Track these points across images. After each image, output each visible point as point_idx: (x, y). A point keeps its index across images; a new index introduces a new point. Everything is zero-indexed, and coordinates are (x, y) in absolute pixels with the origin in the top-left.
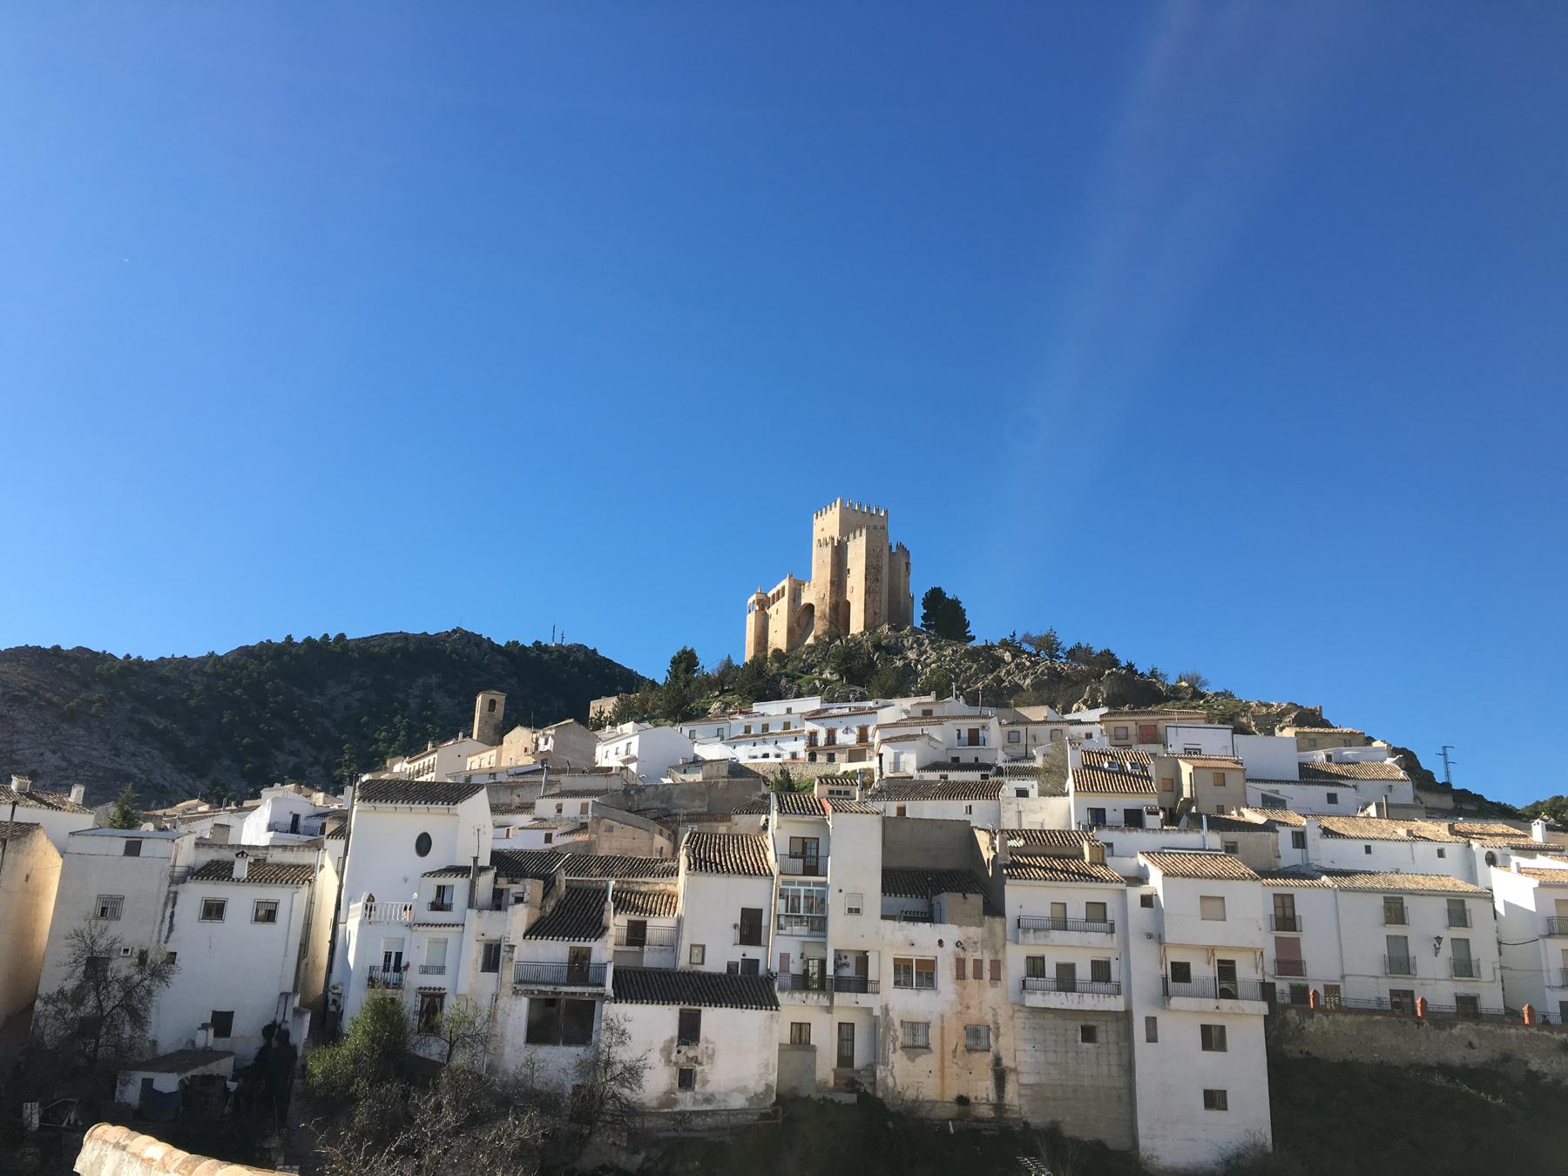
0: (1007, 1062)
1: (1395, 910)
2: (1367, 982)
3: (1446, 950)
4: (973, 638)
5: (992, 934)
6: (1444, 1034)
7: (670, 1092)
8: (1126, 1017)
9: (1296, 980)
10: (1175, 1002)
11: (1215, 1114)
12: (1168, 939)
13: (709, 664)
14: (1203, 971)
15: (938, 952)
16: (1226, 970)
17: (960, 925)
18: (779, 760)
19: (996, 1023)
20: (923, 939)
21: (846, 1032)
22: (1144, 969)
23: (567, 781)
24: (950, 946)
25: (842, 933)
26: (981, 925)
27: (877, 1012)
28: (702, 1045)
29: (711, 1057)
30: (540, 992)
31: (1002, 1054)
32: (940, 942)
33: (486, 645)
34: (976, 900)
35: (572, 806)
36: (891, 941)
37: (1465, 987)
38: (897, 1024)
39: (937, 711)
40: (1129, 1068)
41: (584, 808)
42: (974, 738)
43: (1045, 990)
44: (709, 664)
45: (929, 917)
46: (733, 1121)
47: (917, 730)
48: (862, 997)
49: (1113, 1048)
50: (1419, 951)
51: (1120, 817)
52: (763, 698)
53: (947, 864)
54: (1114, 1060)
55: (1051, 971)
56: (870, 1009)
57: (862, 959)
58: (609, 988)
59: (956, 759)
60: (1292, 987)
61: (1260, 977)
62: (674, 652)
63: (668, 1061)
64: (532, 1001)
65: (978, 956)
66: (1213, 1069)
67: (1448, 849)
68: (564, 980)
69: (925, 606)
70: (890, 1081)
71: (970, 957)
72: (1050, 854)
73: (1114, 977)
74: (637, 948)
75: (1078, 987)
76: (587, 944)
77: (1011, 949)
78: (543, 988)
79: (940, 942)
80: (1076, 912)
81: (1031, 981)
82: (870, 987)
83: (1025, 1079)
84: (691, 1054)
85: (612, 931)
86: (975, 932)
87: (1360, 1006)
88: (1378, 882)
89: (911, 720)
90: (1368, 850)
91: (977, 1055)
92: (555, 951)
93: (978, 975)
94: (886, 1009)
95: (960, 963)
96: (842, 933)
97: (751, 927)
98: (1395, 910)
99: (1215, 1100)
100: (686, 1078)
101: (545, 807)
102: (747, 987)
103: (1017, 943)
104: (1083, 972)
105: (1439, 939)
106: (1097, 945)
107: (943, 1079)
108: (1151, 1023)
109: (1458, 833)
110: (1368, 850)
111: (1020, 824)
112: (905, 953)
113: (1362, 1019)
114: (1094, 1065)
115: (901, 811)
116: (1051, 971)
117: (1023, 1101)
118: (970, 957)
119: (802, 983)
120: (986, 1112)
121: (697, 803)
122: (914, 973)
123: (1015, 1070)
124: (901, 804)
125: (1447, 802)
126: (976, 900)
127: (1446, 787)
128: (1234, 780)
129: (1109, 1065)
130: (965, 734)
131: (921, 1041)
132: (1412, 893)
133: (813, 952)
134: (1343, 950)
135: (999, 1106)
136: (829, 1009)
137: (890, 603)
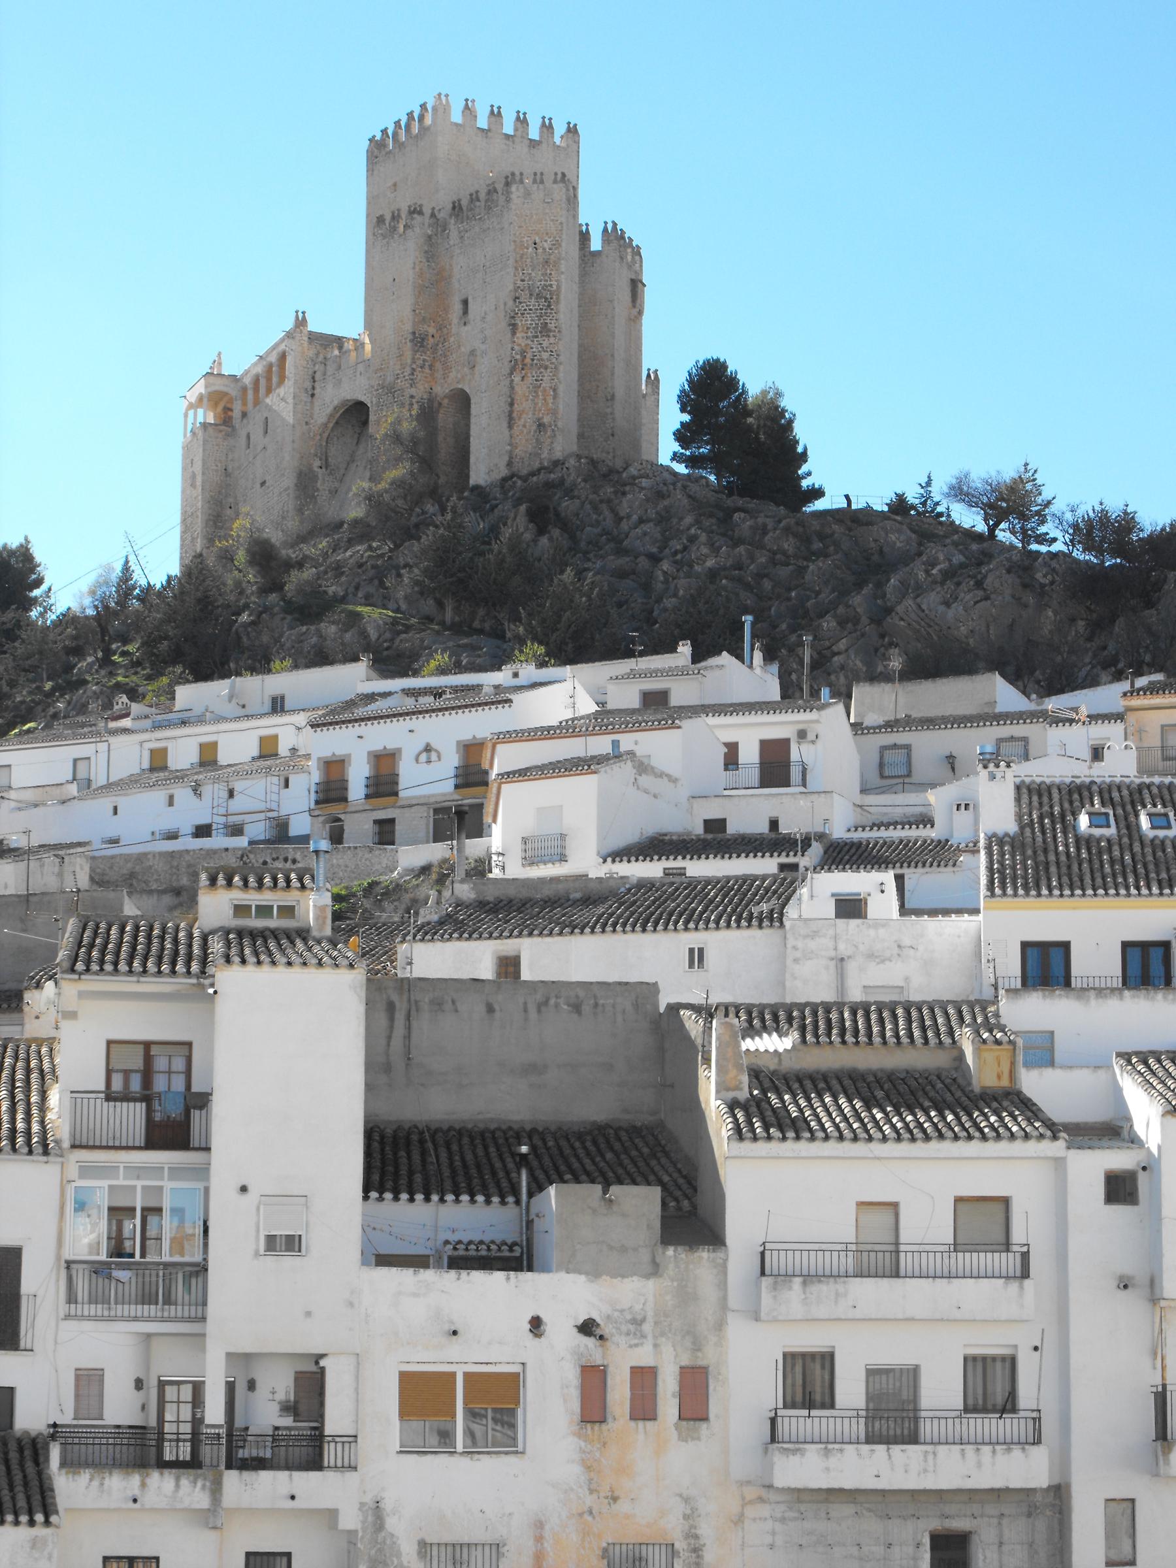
4: (817, 493)
5: (686, 1295)
8: (1056, 1500)
17: (595, 1274)
20: (487, 1318)
25: (253, 1310)
26: (655, 1270)
27: (350, 1520)
32: (536, 1324)
34: (641, 1203)
39: (682, 693)
42: (776, 767)
43: (827, 1443)
45: (516, 1257)
47: (600, 745)
48: (305, 1483)
53: (594, 1107)
55: (851, 1390)
56: (332, 1515)
57: (311, 1385)
59: (715, 826)
65: (644, 1356)
69: (685, 403)
71: (622, 1360)
73: (1026, 1397)
75: (927, 1429)
77: (738, 1331)
79: (536, 1324)
80: (928, 1223)
81: (795, 1422)
82: (330, 1453)
86: (632, 1293)
89: (604, 719)
93: (644, 1409)
94: (376, 1513)
95: (593, 1379)
96: (253, 1310)
104: (942, 1389)
108: (1123, 1515)
111: (841, 986)
112: (431, 1358)
115: (509, 966)
118: (622, 1360)
119: (141, 1449)
122: (468, 1409)
124: (508, 946)
126: (641, 1203)
130: (749, 754)
136: (211, 1517)
137: (585, 395)
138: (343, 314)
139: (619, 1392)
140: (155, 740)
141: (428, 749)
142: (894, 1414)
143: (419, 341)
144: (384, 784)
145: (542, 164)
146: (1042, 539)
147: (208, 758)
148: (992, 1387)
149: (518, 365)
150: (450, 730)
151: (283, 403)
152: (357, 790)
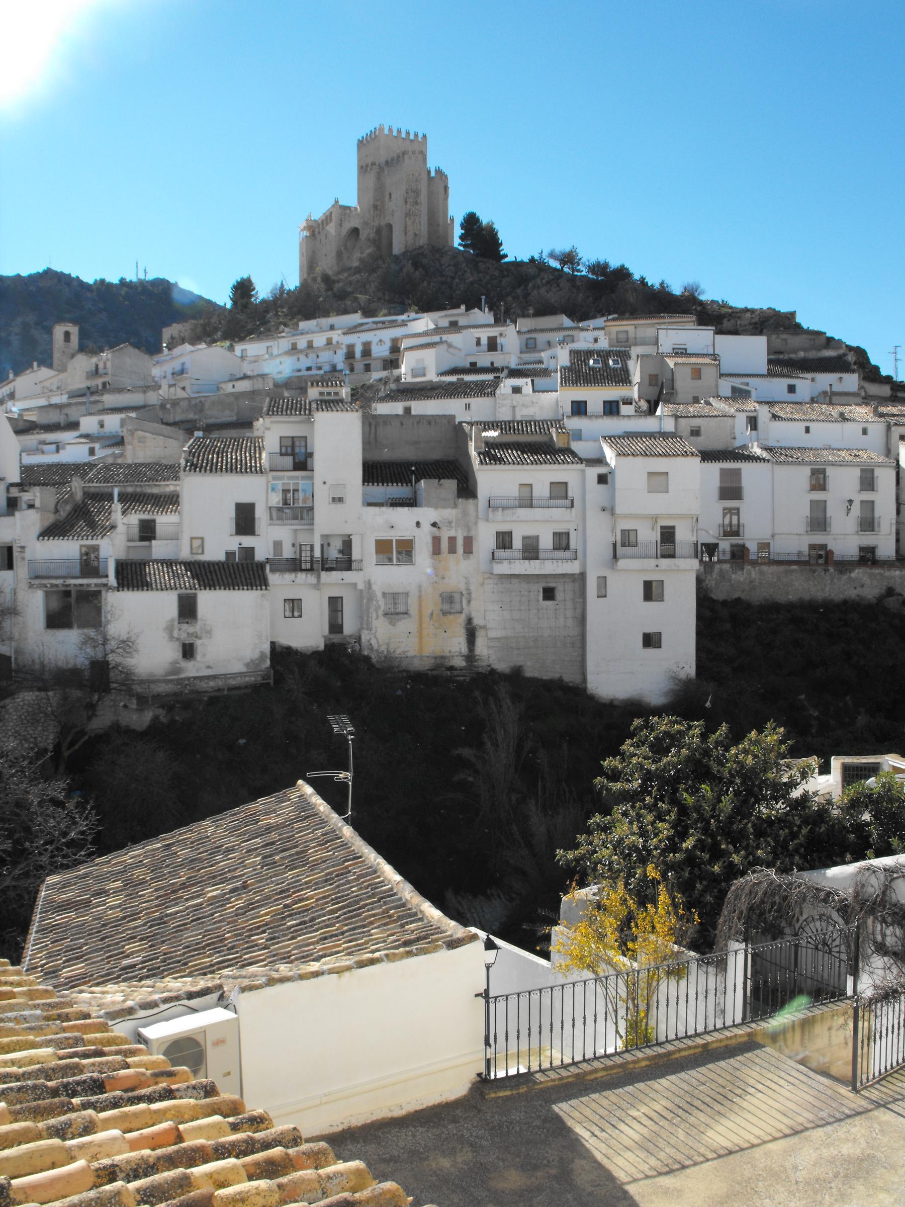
0: (477, 621)
1: (819, 481)
2: (793, 540)
3: (856, 510)
5: (465, 514)
6: (845, 577)
7: (175, 662)
8: (581, 578)
9: (735, 540)
10: (622, 563)
11: (651, 651)
12: (618, 510)
13: (263, 291)
14: (649, 536)
15: (416, 532)
16: (668, 535)
17: (436, 507)
18: (322, 372)
19: (468, 589)
20: (402, 522)
21: (335, 604)
22: (597, 536)
23: (109, 399)
24: (426, 527)
25: (328, 521)
27: (361, 586)
28: (199, 622)
29: (209, 633)
30: (52, 585)
31: (473, 615)
32: (418, 524)
33: (75, 283)
34: (451, 485)
35: (113, 422)
36: (371, 522)
37: (868, 540)
38: (379, 595)
39: (462, 322)
40: (582, 620)
41: (123, 423)
42: (493, 345)
44: (263, 291)
45: (412, 502)
46: (233, 682)
47: (436, 339)
48: (346, 575)
49: (569, 604)
50: (835, 512)
51: (600, 409)
52: (308, 317)
53: (436, 455)
54: (569, 613)
55: (517, 543)
56: (355, 585)
57: (347, 544)
58: (112, 580)
59: (473, 364)
60: (732, 546)
61: (695, 539)
62: (233, 282)
63: (171, 638)
64: (47, 595)
65: (452, 533)
66: (651, 617)
67: (871, 428)
68: (78, 573)
69: (463, 226)
70: (373, 642)
72: (535, 444)
73: (572, 545)
74: (146, 543)
75: (541, 555)
76: (94, 542)
77: (482, 525)
78: (54, 582)
79: (418, 524)
81: (500, 553)
82: (354, 565)
83: (492, 634)
84: (191, 630)
85: (121, 528)
86: (448, 513)
87: (781, 558)
88: (810, 457)
89: (438, 330)
90: (807, 430)
91: (451, 617)
92: (67, 549)
93: (452, 550)
94: (369, 584)
95: (436, 541)
96: (328, 521)
97: (245, 520)
98: (819, 481)
99: (651, 641)
100: (188, 651)
101: (89, 424)
102: (243, 572)
103: (487, 520)
104: (546, 543)
105: (850, 502)
106: (556, 518)
107: (421, 638)
109: (882, 415)
110: (807, 430)
112: (385, 535)
113: (782, 568)
114: (553, 619)
115: (408, 410)
116: (517, 543)
117: (491, 652)
119: (294, 565)
120: (459, 662)
121: (227, 412)
122: (397, 551)
123: (484, 627)
124: (407, 404)
125: (886, 390)
126: (451, 485)
127: (888, 380)
128: (709, 374)
129: (566, 618)
130: (484, 341)
131: (401, 608)
132: (833, 464)
133: (303, 539)
134: (775, 511)
135: (470, 657)
136: (317, 586)
138: (350, 199)
139: (445, 545)
140: (293, 340)
141: (381, 341)
142: (531, 551)
143: (375, 207)
144: (367, 352)
145: (412, 149)
146: (578, 271)
147: (310, 345)
148: (562, 541)
149: (408, 215)
150: (388, 335)
151: (331, 228)
152: (358, 354)
